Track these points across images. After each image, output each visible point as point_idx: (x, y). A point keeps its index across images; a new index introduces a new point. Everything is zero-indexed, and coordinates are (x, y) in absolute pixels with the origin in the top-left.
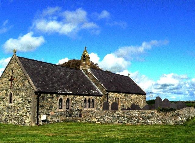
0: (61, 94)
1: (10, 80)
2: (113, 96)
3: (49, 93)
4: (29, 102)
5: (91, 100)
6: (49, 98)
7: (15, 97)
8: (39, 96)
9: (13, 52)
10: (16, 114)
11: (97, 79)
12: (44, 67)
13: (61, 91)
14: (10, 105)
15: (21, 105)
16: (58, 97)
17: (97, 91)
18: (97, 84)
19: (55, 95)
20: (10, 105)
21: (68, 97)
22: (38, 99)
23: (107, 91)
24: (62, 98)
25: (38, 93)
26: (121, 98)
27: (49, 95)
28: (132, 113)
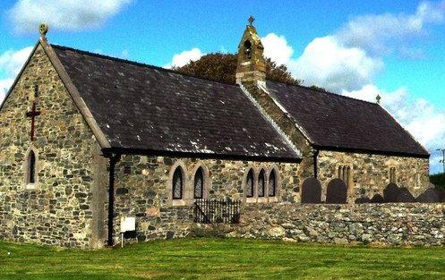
0: (180, 155)
1: (28, 114)
2: (333, 161)
3: (144, 152)
4: (85, 179)
5: (268, 174)
6: (143, 166)
7: (43, 165)
8: (113, 162)
10: (46, 213)
11: (285, 111)
12: (128, 75)
13: (178, 147)
14: (31, 187)
15: (62, 188)
16: (169, 163)
17: (285, 146)
18: (285, 125)
19: (160, 159)
20: (31, 187)
21: (200, 163)
22: (111, 169)
23: (314, 146)
24: (183, 166)
26: (355, 168)
27: (144, 159)
28: (388, 211)
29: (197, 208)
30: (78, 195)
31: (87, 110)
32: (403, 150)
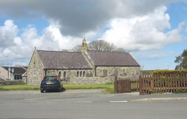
0: (60, 69)
1: (34, 63)
2: (101, 69)
3: (52, 69)
4: (42, 74)
5: (83, 72)
6: (52, 72)
7: (36, 72)
8: (46, 71)
9: (34, 48)
10: (37, 80)
11: (90, 58)
12: (53, 54)
13: (60, 68)
14: (35, 76)
15: (39, 76)
16: (58, 71)
17: (89, 66)
18: (90, 61)
19: (56, 70)
20: (35, 76)
21: (65, 70)
22: (46, 73)
23: (95, 66)
24: (61, 71)
25: (46, 70)
26: (109, 70)
27: (52, 70)
28: (89, 78)
29: (64, 79)
30: (41, 77)
31: (42, 62)
32: (136, 65)
